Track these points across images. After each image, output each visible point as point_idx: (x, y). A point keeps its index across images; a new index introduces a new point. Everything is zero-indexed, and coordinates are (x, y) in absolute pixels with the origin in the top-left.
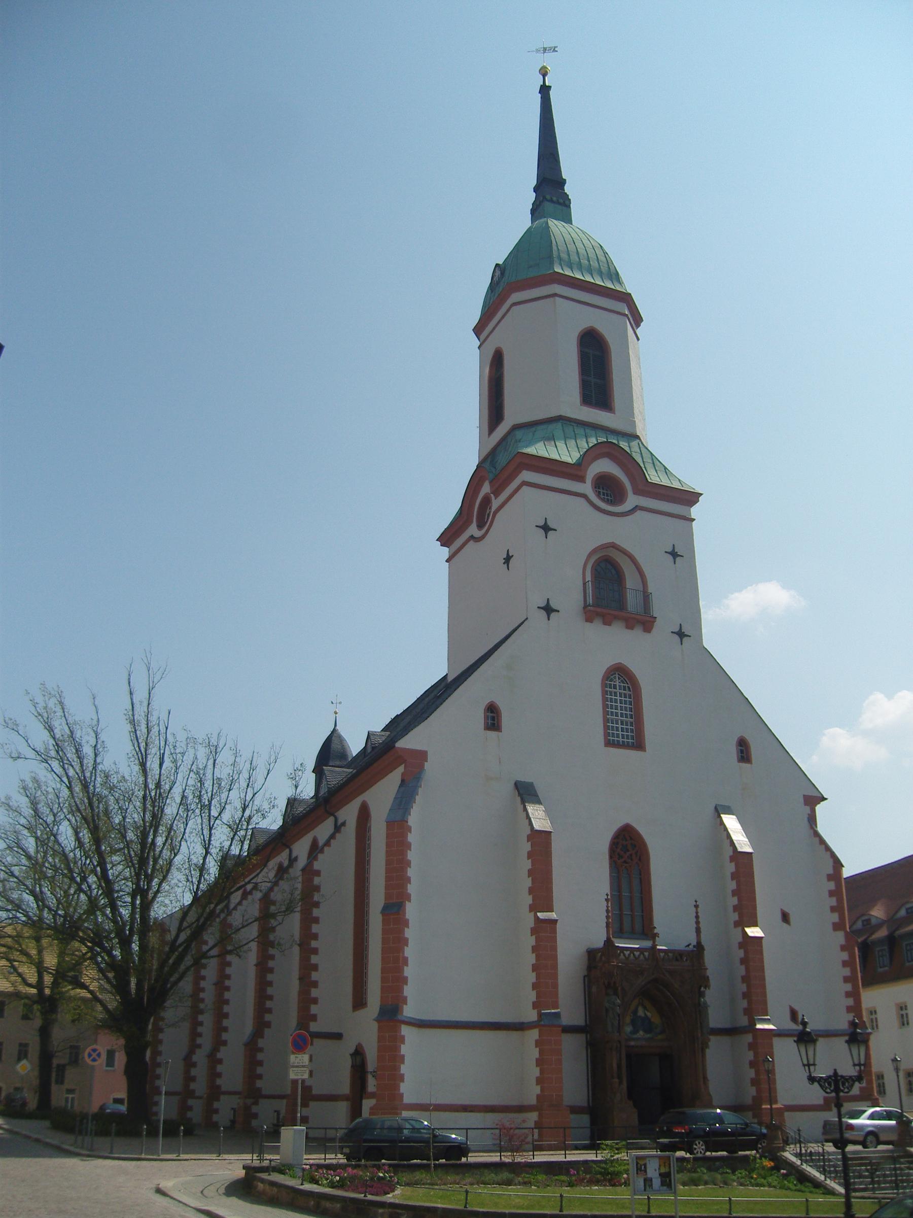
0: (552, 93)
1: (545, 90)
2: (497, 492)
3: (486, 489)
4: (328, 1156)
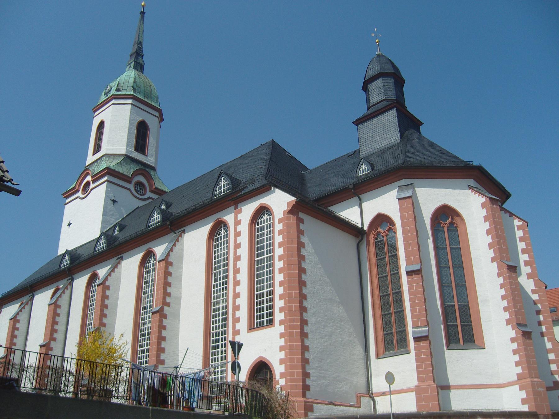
0: (145, 15)
2: (94, 182)
3: (89, 178)
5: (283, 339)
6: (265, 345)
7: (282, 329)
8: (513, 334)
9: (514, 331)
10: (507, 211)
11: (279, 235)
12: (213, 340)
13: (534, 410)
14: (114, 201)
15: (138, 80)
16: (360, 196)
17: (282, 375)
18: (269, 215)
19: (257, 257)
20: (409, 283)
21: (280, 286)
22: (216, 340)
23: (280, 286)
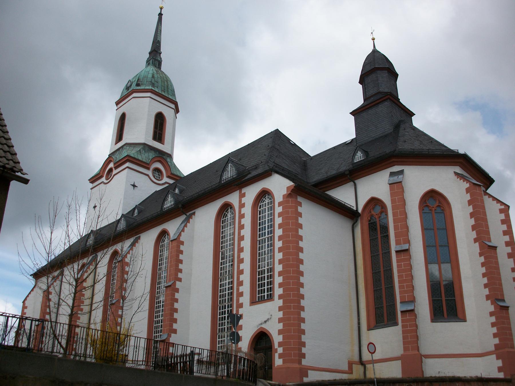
0: (163, 16)
1: (160, 15)
2: (116, 168)
3: (111, 165)
4: (99, 332)
5: (282, 312)
6: (257, 317)
7: (280, 303)
8: (492, 308)
9: (493, 306)
10: (490, 196)
11: (279, 217)
12: (220, 312)
13: (509, 377)
14: (134, 186)
15: (156, 76)
16: (356, 181)
17: (280, 344)
18: (270, 199)
19: (259, 237)
20: (398, 261)
21: (279, 264)
22: (222, 312)
23: (279, 264)
